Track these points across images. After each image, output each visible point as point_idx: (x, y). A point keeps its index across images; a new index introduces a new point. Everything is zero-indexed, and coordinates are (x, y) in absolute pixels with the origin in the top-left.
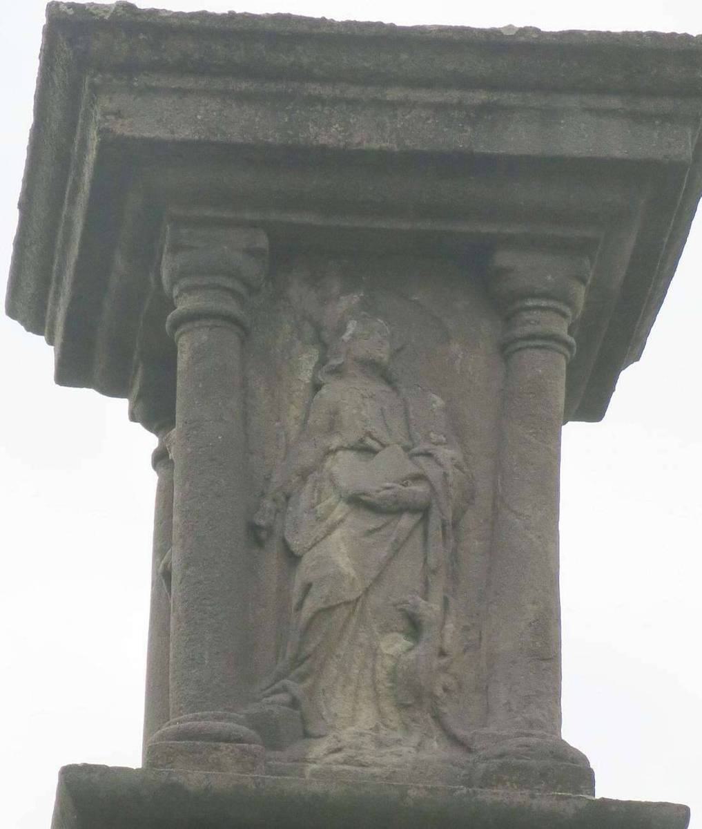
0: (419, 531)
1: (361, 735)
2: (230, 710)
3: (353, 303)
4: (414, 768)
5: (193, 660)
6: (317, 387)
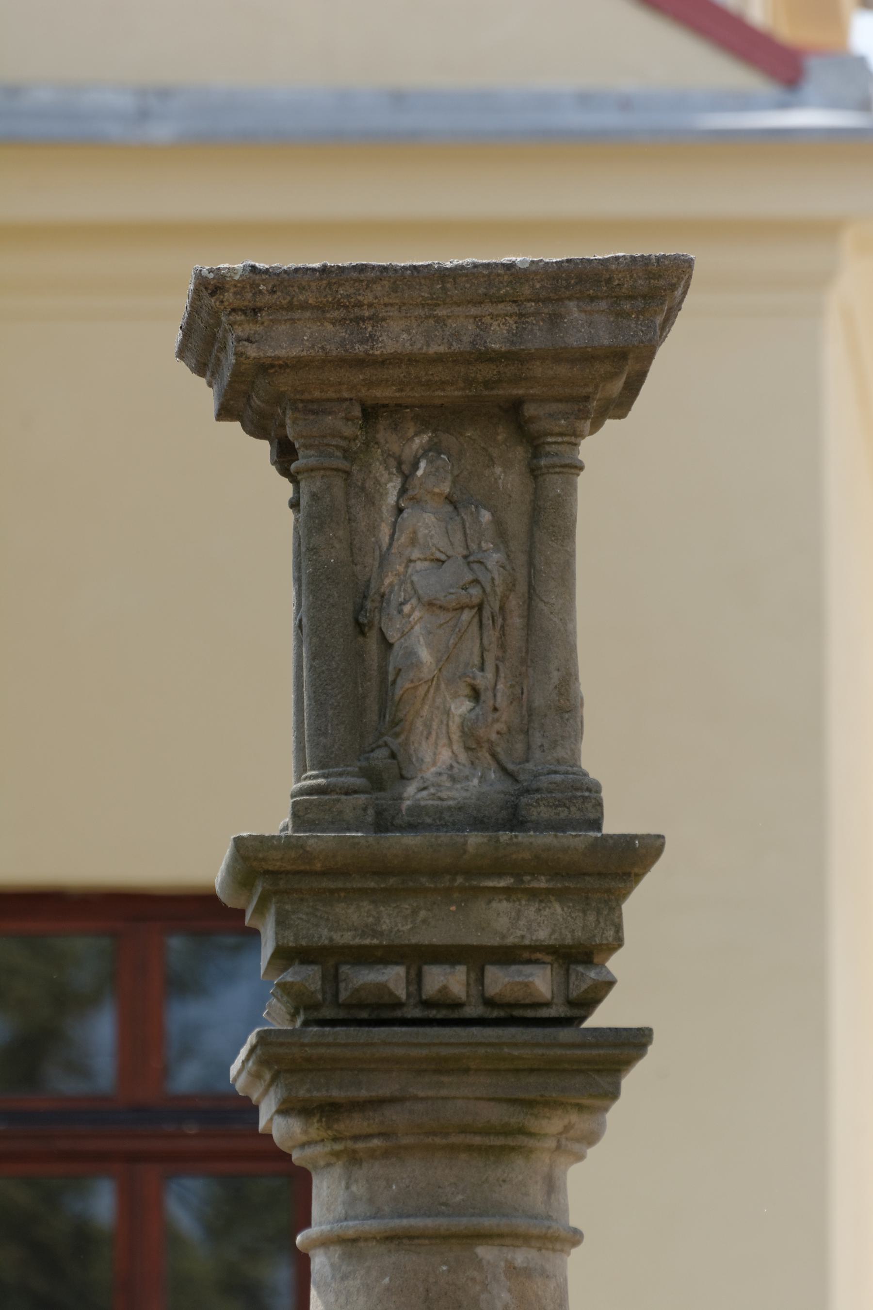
0: (476, 620)
1: (440, 774)
2: (348, 766)
3: (424, 442)
4: (478, 799)
5: (320, 730)
6: (400, 511)
